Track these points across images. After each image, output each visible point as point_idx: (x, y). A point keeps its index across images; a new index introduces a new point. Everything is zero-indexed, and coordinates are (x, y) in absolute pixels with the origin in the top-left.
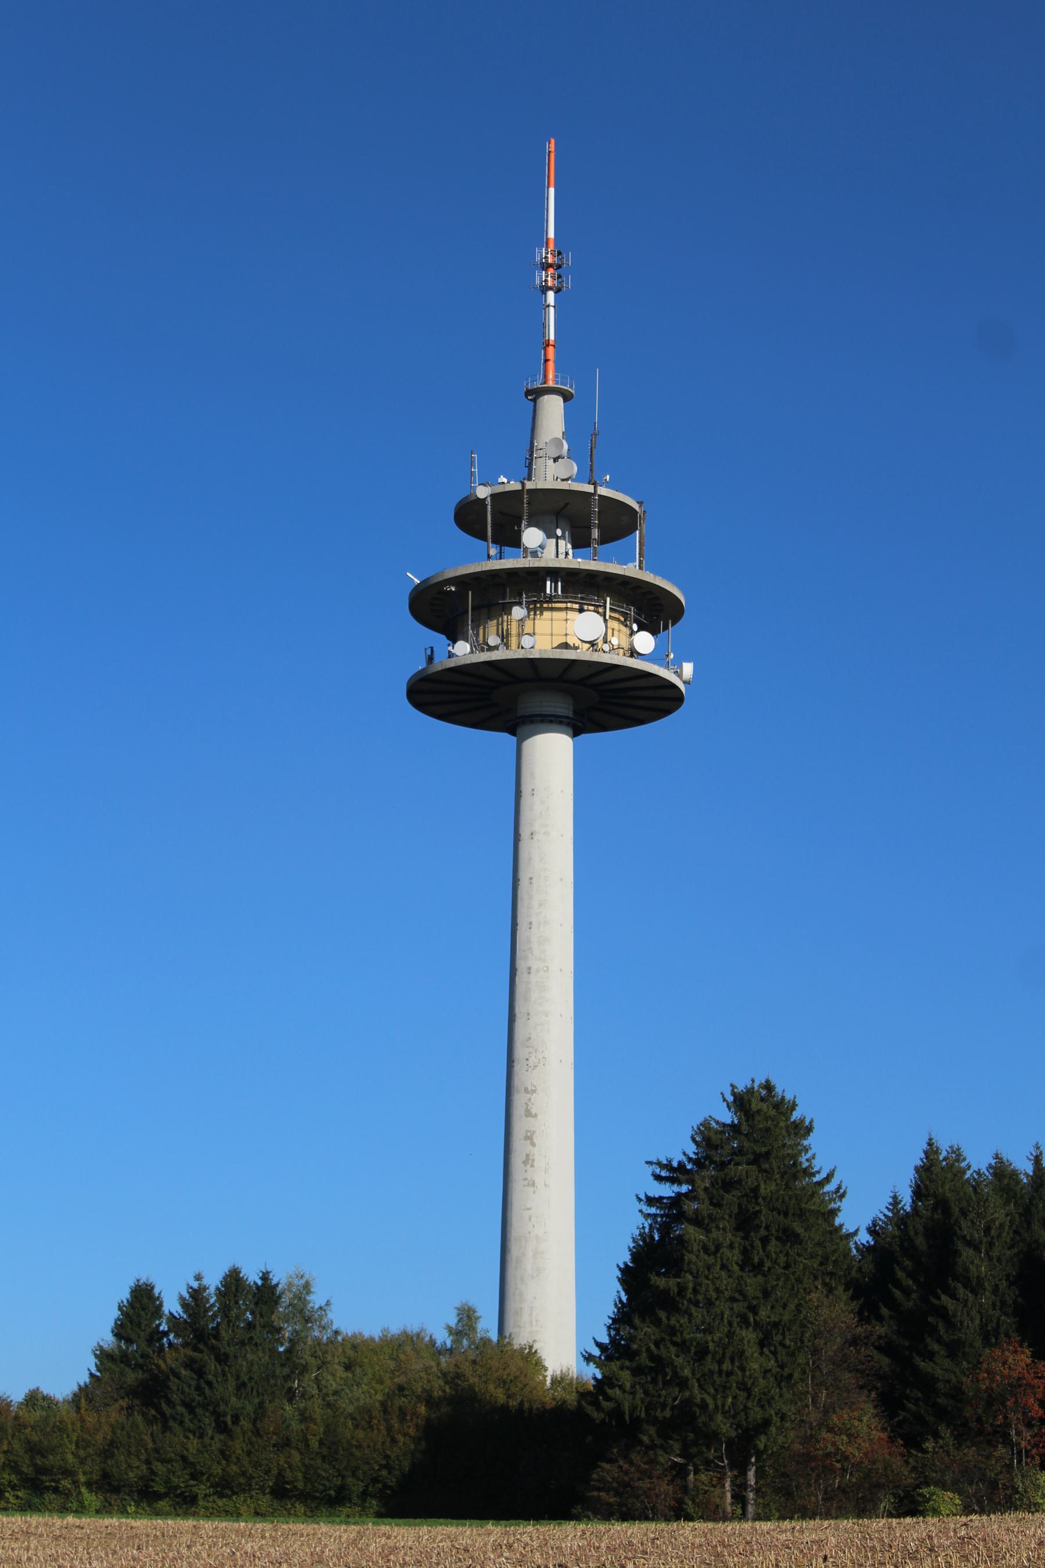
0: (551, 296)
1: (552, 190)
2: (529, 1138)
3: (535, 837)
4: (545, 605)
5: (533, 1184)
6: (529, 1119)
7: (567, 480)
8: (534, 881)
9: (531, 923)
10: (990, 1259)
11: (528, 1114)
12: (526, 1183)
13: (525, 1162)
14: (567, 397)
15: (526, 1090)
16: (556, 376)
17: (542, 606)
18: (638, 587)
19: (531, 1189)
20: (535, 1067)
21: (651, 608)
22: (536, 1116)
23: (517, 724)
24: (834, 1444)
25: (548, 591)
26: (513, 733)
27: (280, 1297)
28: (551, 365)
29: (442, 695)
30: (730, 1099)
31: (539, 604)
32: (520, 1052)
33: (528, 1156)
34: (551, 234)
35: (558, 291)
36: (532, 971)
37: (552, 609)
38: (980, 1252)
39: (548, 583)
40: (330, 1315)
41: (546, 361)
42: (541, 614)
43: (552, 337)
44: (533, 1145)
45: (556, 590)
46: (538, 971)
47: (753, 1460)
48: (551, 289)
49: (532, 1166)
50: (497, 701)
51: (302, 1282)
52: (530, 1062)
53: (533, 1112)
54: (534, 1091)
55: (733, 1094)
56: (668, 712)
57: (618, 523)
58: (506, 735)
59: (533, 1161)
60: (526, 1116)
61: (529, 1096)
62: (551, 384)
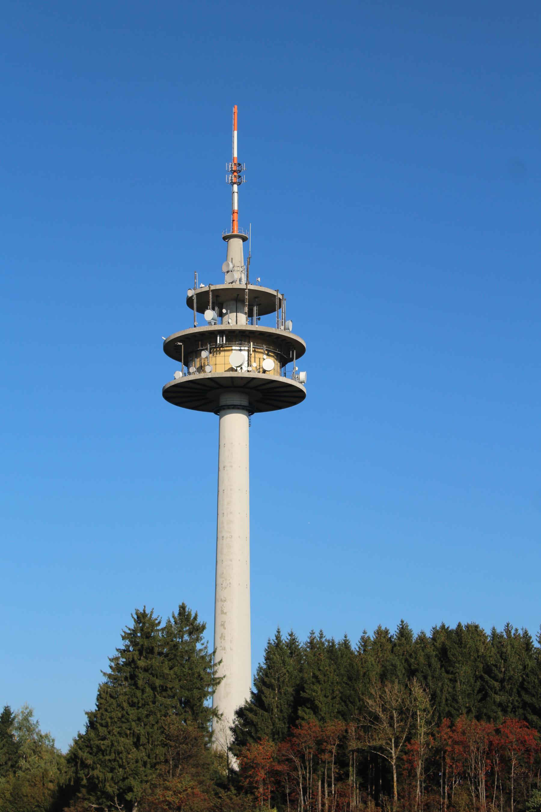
0: (235, 186)
1: (236, 133)
2: (223, 625)
3: (226, 468)
4: (221, 349)
5: (225, 649)
6: (223, 615)
7: (232, 283)
8: (225, 491)
9: (223, 514)
10: (280, 693)
11: (223, 612)
12: (221, 648)
13: (221, 638)
14: (244, 239)
15: (221, 600)
16: (238, 229)
17: (220, 349)
18: (285, 340)
19: (224, 651)
20: (226, 588)
21: (285, 350)
22: (226, 613)
23: (219, 409)
24: (164, 796)
25: (218, 342)
26: (216, 413)
27: (13, 719)
28: (235, 222)
29: (178, 395)
30: (135, 617)
31: (215, 349)
32: (219, 581)
33: (222, 634)
34: (236, 155)
35: (239, 184)
36: (224, 538)
37: (225, 351)
38: (275, 690)
39: (218, 338)
40: (40, 728)
41: (233, 221)
42: (220, 353)
43: (236, 208)
44: (225, 628)
45: (223, 341)
46: (227, 538)
47: (136, 804)
48: (235, 183)
49: (224, 639)
50: (206, 397)
51: (28, 710)
52: (223, 586)
53: (225, 611)
54: (225, 601)
55: (137, 614)
56: (295, 403)
57: (263, 304)
58: (212, 414)
59: (225, 637)
60: (222, 614)
61: (222, 603)
62: (236, 233)
